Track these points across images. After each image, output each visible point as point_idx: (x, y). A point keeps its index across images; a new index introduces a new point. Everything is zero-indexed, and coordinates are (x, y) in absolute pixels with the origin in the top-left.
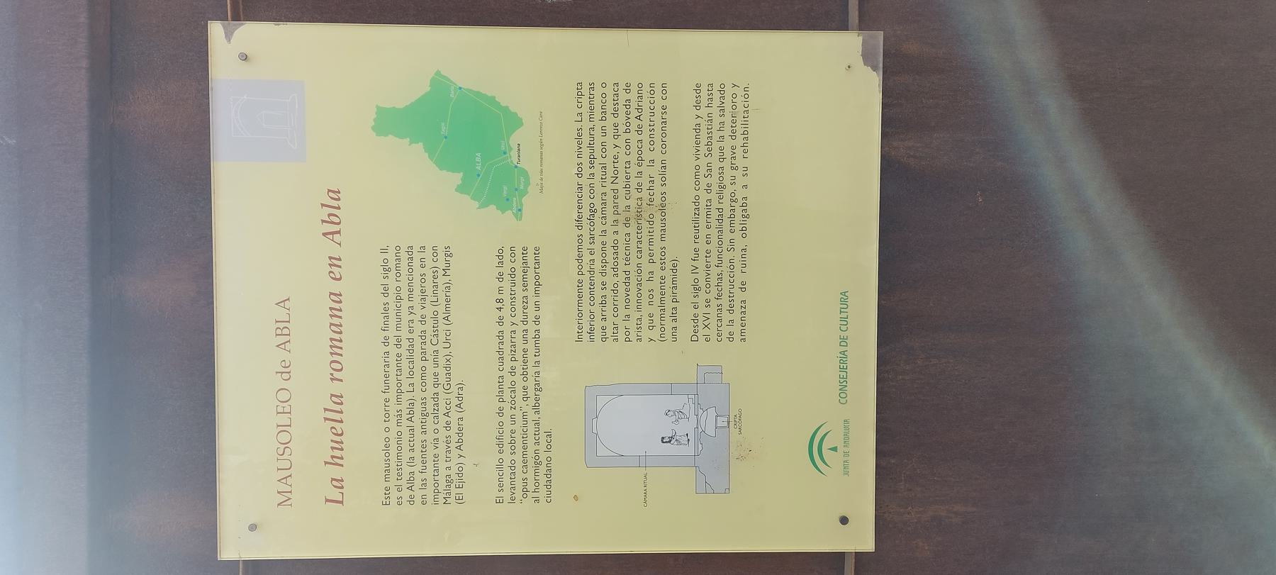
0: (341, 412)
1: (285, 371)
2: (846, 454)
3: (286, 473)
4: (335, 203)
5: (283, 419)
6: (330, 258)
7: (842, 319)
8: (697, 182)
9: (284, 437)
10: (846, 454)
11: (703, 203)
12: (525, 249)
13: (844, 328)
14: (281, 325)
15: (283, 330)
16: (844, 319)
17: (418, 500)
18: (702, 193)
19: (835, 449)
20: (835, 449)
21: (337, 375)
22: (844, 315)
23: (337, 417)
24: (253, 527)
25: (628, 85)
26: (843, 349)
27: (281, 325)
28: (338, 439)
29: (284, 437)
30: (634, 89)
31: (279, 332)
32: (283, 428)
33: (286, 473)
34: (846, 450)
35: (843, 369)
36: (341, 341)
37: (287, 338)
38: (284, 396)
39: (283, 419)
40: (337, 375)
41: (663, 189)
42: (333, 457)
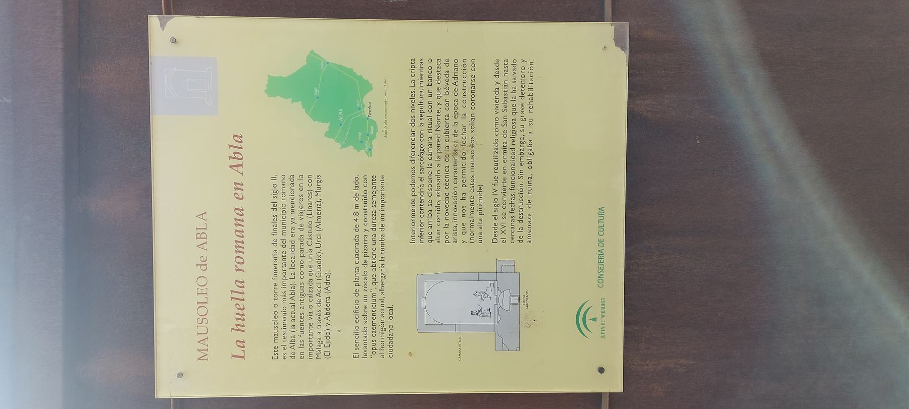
0: (243, 293)
1: (203, 264)
2: (603, 323)
3: (204, 337)
4: (239, 145)
5: (202, 298)
6: (235, 183)
7: (600, 227)
8: (497, 130)
9: (202, 311)
10: (603, 323)
11: (501, 145)
12: (374, 177)
13: (601, 233)
14: (201, 231)
15: (201, 234)
16: (602, 227)
17: (298, 355)
18: (500, 138)
19: (595, 319)
20: (595, 319)
21: (240, 267)
22: (601, 224)
23: (240, 296)
24: (180, 375)
25: (447, 61)
26: (601, 248)
27: (201, 231)
28: (241, 312)
29: (202, 311)
30: (452, 63)
31: (199, 236)
32: (202, 304)
33: (204, 337)
34: (603, 320)
35: (600, 263)
36: (243, 242)
37: (204, 241)
38: (202, 281)
39: (202, 298)
40: (240, 267)
41: (473, 135)
42: (237, 325)
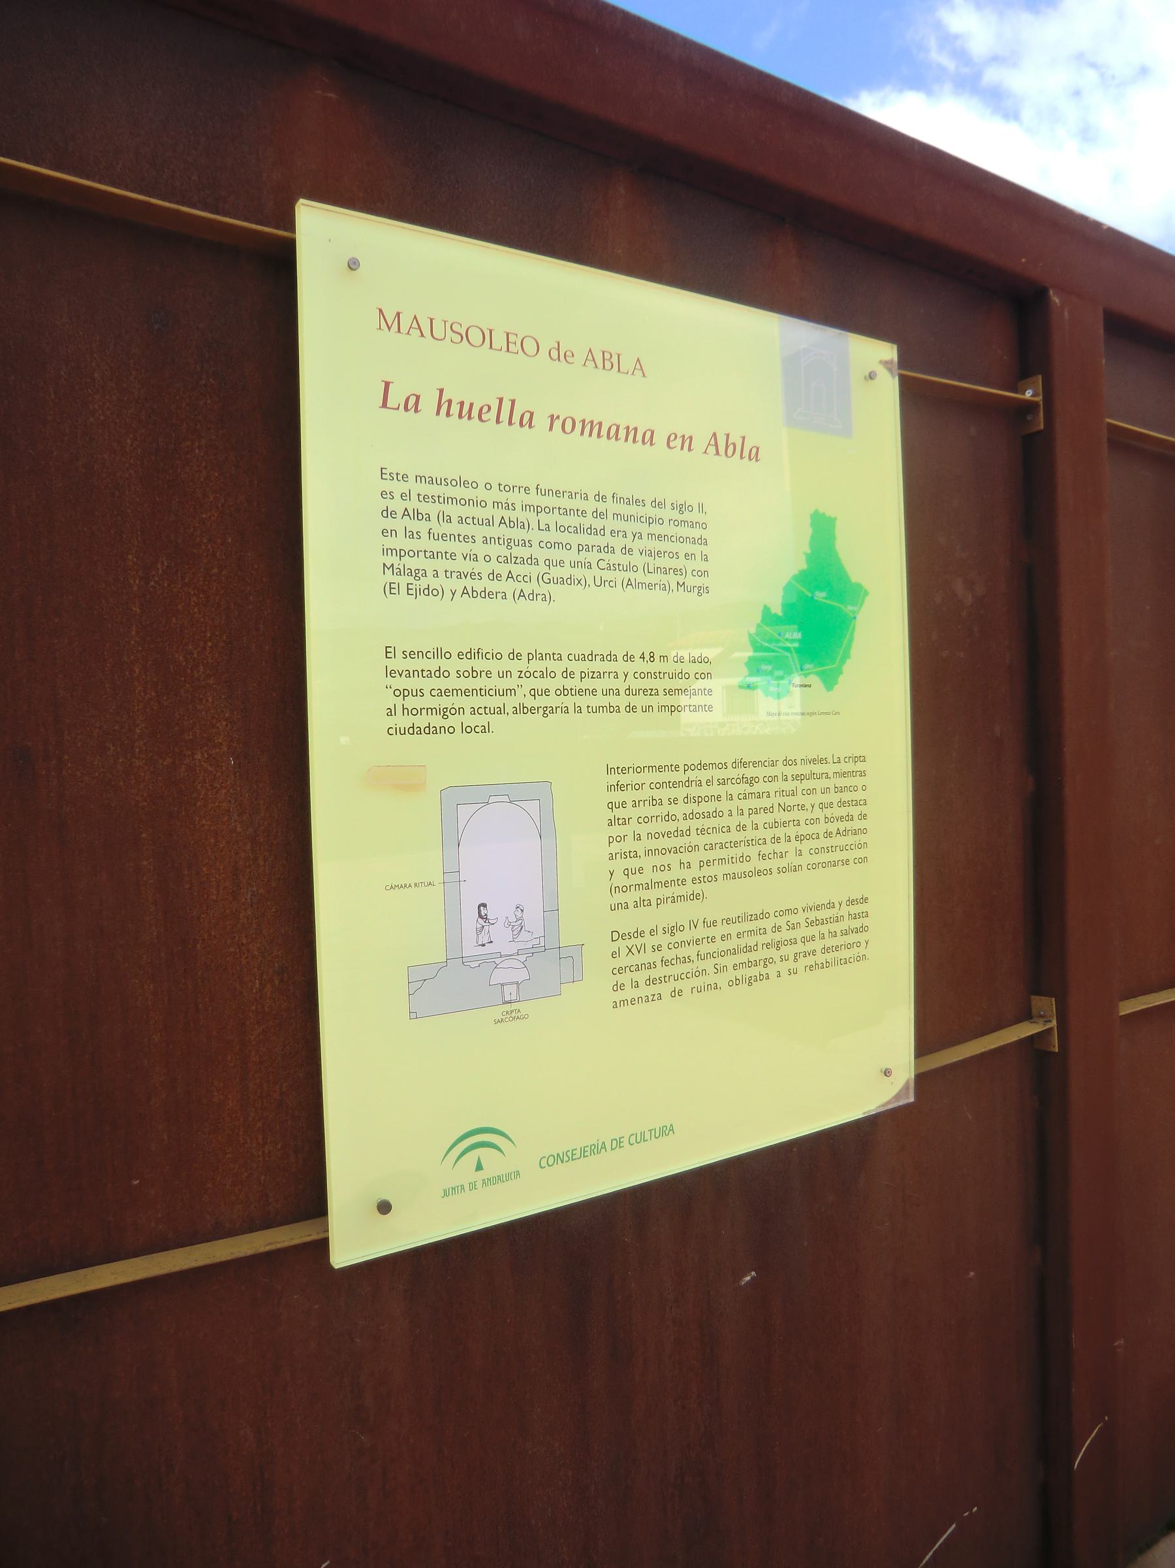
2: (473, 1186)
3: (427, 332)
4: (516, 419)
6: (691, 438)
7: (643, 1134)
9: (475, 336)
10: (473, 1186)
15: (608, 361)
17: (389, 524)
19: (479, 1167)
20: (479, 1167)
28: (475, 413)
31: (607, 356)
32: (487, 336)
33: (427, 332)
34: (479, 1184)
35: (583, 1152)
37: (600, 365)
38: (530, 346)
39: (499, 340)
40: (558, 424)
42: (450, 402)
